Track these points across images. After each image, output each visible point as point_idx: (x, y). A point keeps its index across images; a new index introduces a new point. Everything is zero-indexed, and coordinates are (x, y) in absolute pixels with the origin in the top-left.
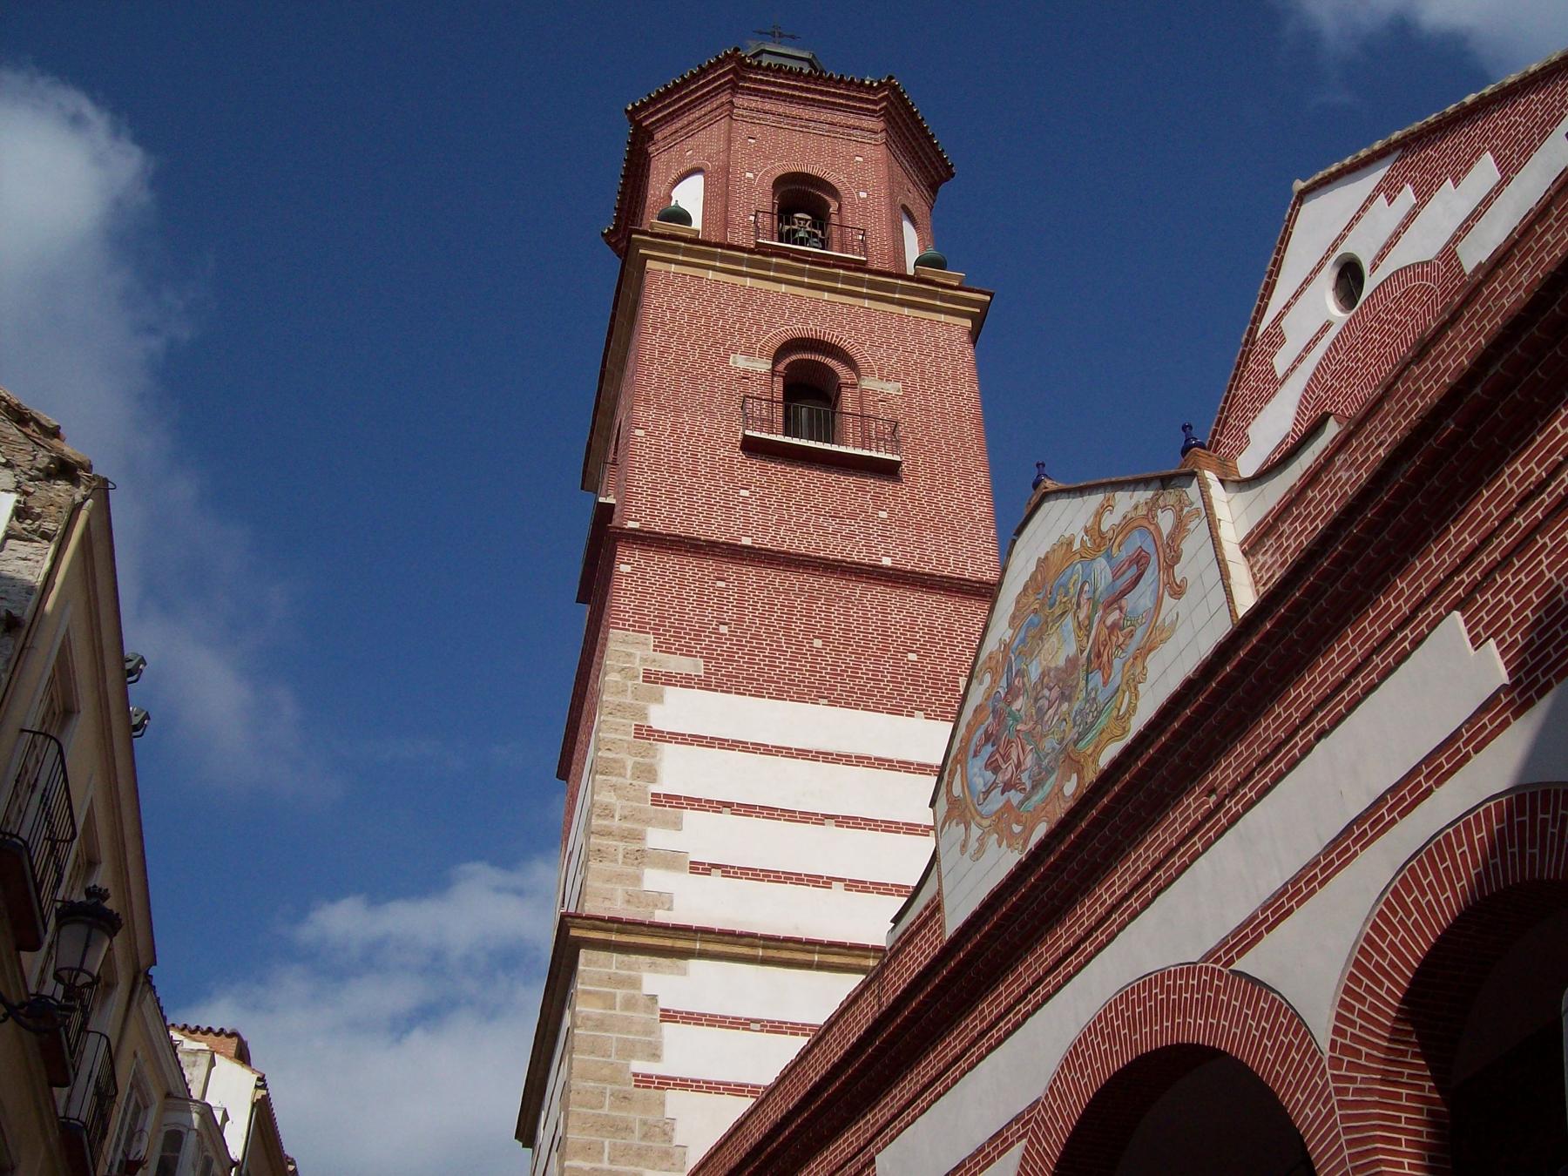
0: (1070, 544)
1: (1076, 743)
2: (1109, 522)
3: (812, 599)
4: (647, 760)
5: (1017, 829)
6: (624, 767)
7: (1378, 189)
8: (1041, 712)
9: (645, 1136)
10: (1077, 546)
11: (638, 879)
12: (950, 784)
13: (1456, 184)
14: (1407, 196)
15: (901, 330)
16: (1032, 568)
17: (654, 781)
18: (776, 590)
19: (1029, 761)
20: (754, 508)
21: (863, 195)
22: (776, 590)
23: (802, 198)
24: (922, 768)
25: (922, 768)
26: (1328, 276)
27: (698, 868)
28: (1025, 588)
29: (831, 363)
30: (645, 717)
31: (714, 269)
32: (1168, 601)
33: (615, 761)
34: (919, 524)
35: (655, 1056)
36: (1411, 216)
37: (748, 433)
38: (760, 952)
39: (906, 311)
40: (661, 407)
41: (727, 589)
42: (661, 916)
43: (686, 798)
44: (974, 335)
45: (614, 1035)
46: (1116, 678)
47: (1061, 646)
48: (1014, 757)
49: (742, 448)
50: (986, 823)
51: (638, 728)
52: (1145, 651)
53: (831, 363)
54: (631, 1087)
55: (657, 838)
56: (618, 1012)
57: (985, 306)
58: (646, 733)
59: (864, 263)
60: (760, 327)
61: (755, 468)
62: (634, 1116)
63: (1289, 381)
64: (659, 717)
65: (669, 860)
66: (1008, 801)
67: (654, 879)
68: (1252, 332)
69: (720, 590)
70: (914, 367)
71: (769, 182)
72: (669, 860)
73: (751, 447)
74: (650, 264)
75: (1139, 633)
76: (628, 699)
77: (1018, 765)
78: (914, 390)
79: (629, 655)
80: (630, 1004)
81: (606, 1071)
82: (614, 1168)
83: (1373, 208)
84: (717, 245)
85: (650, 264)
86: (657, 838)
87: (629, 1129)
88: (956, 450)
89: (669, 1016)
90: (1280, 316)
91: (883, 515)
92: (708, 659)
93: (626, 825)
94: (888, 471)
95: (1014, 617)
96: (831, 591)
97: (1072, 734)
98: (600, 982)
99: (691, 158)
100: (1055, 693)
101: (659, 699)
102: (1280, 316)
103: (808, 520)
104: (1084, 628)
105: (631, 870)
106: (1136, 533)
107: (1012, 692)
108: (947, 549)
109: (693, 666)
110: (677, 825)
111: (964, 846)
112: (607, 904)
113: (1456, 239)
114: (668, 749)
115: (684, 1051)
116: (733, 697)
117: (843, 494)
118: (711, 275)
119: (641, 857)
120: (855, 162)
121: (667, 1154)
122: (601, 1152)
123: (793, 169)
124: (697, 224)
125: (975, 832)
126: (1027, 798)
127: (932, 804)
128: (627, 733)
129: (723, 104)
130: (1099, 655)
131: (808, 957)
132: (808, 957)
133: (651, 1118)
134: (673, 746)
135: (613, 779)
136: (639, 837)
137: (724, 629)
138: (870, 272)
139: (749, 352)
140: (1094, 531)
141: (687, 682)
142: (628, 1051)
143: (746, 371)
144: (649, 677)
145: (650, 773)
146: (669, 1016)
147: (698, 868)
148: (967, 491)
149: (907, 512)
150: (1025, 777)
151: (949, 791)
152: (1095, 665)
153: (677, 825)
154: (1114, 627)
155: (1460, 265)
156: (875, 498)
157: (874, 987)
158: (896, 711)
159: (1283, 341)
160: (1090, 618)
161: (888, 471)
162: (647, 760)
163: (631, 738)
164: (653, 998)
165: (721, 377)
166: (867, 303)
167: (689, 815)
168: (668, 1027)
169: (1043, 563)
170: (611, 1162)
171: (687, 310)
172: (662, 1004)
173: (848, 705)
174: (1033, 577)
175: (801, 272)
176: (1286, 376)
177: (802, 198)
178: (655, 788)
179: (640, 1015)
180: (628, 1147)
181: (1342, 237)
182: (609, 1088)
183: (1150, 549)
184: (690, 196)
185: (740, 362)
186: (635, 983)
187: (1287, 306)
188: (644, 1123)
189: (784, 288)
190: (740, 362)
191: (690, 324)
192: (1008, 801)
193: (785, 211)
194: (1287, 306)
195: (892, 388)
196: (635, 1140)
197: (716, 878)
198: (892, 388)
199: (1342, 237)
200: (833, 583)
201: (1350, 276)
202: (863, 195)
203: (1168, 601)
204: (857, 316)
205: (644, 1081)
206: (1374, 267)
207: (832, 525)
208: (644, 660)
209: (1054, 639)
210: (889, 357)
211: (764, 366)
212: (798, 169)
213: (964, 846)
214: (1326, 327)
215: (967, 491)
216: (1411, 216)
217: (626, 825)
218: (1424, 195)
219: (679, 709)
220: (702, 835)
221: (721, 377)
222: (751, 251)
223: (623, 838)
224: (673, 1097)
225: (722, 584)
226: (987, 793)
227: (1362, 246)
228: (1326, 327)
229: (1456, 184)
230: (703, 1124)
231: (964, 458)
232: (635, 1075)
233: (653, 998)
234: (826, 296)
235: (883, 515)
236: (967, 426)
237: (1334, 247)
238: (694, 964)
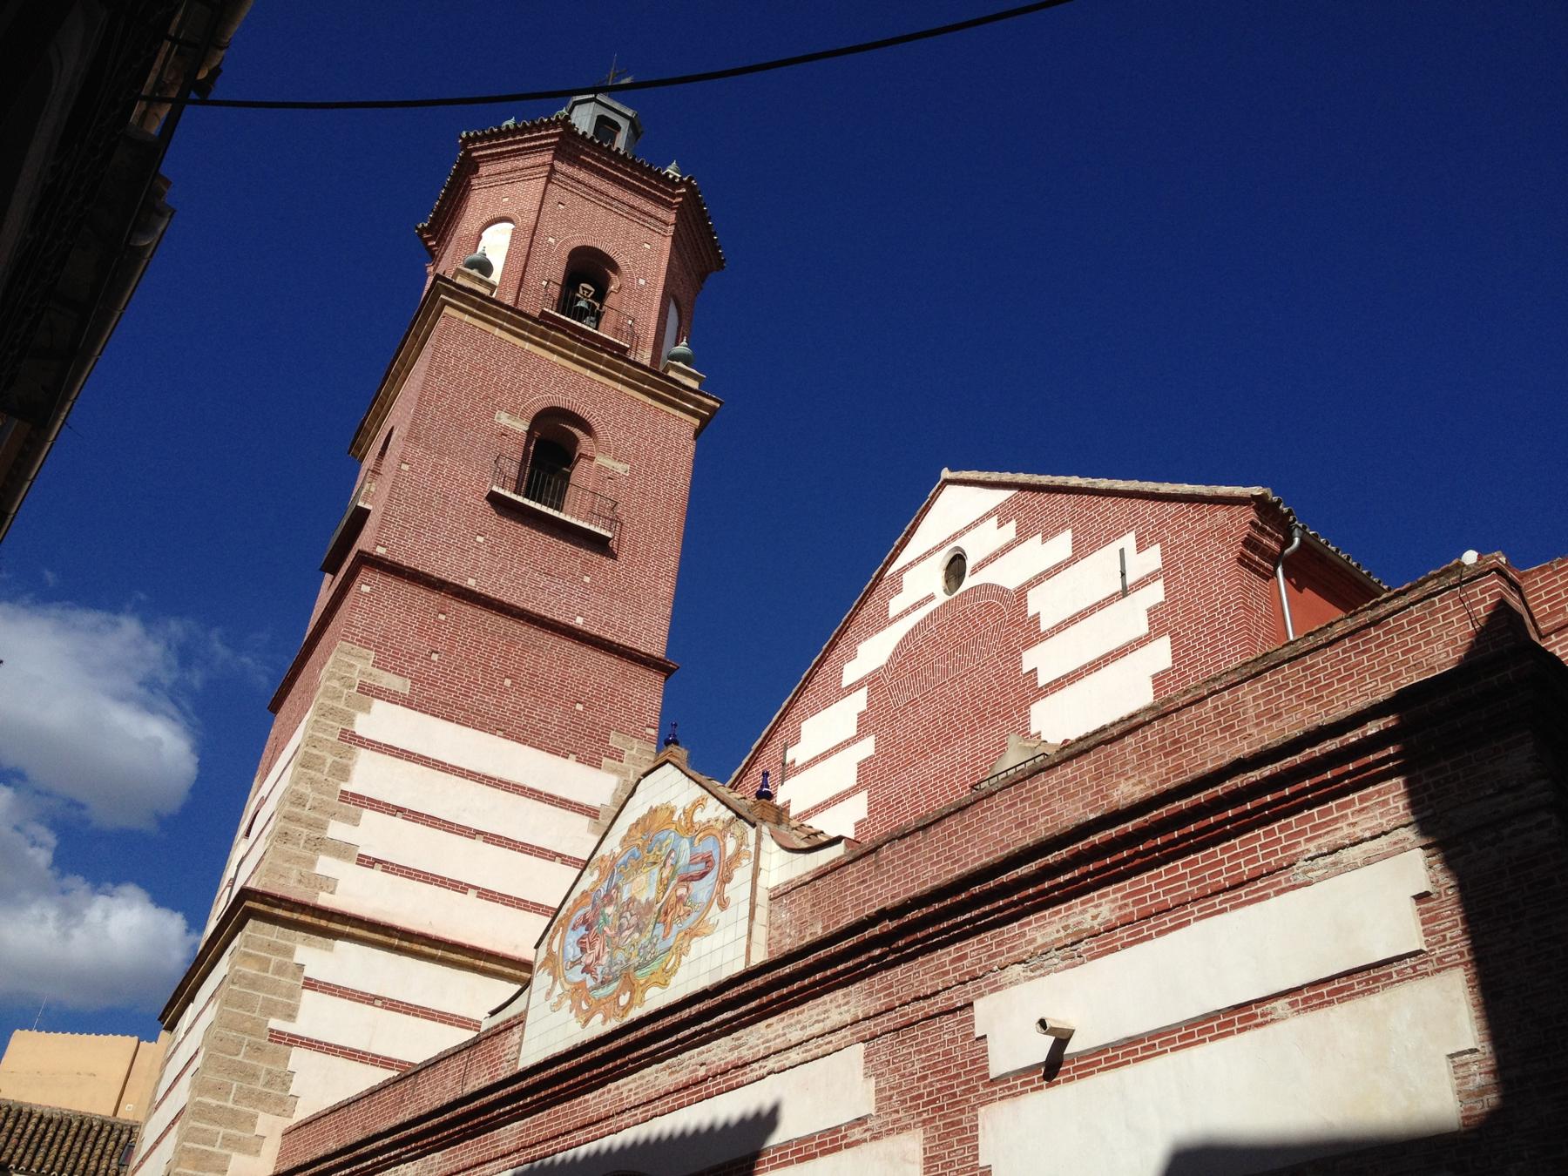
0: (672, 813)
1: (636, 969)
2: (700, 817)
3: (511, 643)
4: (344, 761)
5: (584, 1006)
6: (324, 764)
7: (995, 511)
8: (620, 929)
9: (269, 1084)
10: (675, 818)
11: (313, 863)
12: (552, 938)
13: (1044, 541)
14: (1010, 530)
15: (641, 418)
16: (645, 811)
17: (346, 780)
18: (485, 630)
19: (605, 959)
20: (484, 554)
21: (642, 282)
22: (485, 630)
23: (589, 270)
24: (536, 908)
25: (536, 908)
26: (941, 559)
27: (367, 862)
28: (637, 823)
29: (578, 432)
30: (351, 722)
31: (501, 327)
32: (715, 907)
33: (318, 757)
34: (613, 593)
35: (291, 1016)
36: (1008, 548)
37: (495, 489)
38: (396, 942)
39: (650, 401)
40: (428, 447)
41: (445, 622)
42: (324, 900)
43: (369, 799)
44: (698, 434)
45: (262, 995)
46: (671, 941)
47: (643, 888)
48: (597, 947)
49: (487, 498)
50: (567, 987)
51: (344, 731)
52: (691, 933)
53: (578, 432)
54: (264, 1041)
55: (337, 830)
56: (269, 975)
57: (713, 410)
58: (352, 739)
59: (625, 350)
60: (527, 391)
61: (492, 519)
62: (263, 1066)
63: (895, 625)
64: (364, 725)
65: (342, 851)
66: (584, 981)
67: (326, 865)
68: (884, 570)
69: (441, 622)
70: (642, 457)
71: (566, 251)
72: (342, 851)
73: (495, 500)
74: (447, 310)
75: (694, 915)
76: (341, 705)
77: (597, 958)
78: (639, 473)
79: (351, 666)
80: (281, 969)
81: (248, 1025)
82: (236, 1107)
83: (982, 526)
84: (508, 307)
85: (447, 310)
86: (337, 830)
87: (255, 1076)
88: (658, 533)
89: (311, 984)
90: (904, 569)
91: (587, 579)
92: (414, 681)
93: (313, 814)
94: (599, 544)
95: (624, 839)
96: (529, 638)
97: (635, 961)
98: (261, 948)
99: (505, 204)
100: (633, 920)
101: (367, 709)
102: (904, 569)
103: (526, 573)
104: (664, 885)
105: (308, 854)
106: (711, 839)
107: (609, 899)
108: (630, 619)
109: (399, 684)
110: (355, 821)
111: (549, 994)
112: (282, 881)
113: (1031, 584)
114: (363, 754)
115: (316, 1016)
116: (427, 717)
117: (560, 555)
118: (497, 331)
119: (320, 844)
120: (643, 250)
121: (281, 1102)
122: (228, 1093)
123: (589, 243)
124: (495, 277)
125: (558, 990)
126: (596, 988)
127: (537, 946)
128: (332, 734)
129: (544, 164)
130: (666, 914)
131: (434, 951)
132: (434, 951)
133: (274, 1068)
134: (368, 752)
135: (312, 773)
136: (322, 827)
137: (435, 657)
138: (629, 362)
139: (512, 413)
140: (689, 813)
141: (392, 698)
142: (270, 1009)
143: (506, 428)
144: (364, 689)
145: (343, 772)
146: (311, 984)
147: (367, 862)
148: (658, 571)
149: (607, 581)
150: (599, 970)
151: (550, 944)
152: (662, 918)
153: (355, 821)
154: (680, 899)
155: (1026, 606)
156: (584, 563)
157: (465, 1054)
158: (554, 751)
159: (900, 591)
160: (669, 879)
161: (599, 544)
162: (344, 761)
163: (334, 739)
164: (301, 967)
165: (484, 431)
166: (620, 387)
167: (367, 814)
168: (307, 993)
169: (653, 811)
170: (235, 1102)
171: (471, 359)
172: (307, 973)
173: (518, 740)
174: (644, 818)
175: (572, 348)
176: (895, 620)
177: (589, 270)
178: (345, 786)
179: (286, 980)
180: (251, 1092)
181: (960, 534)
182: (247, 1038)
183: (717, 859)
184: (496, 244)
185: (503, 419)
186: (289, 952)
187: (912, 564)
188: (269, 1072)
189: (555, 358)
190: (503, 419)
191: (469, 374)
192: (584, 981)
193: (572, 278)
194: (912, 564)
195: (621, 468)
196: (259, 1086)
197: (376, 874)
198: (621, 468)
199: (960, 534)
200: (532, 632)
201: (956, 568)
202: (642, 282)
203: (715, 907)
204: (609, 396)
205: (277, 1037)
206: (974, 571)
207: (544, 581)
208: (362, 673)
209: (643, 877)
210: (626, 439)
211: (522, 427)
212: (594, 244)
213: (549, 994)
214: (931, 598)
215: (658, 571)
216: (1008, 548)
217: (313, 814)
218: (1022, 536)
219: (383, 721)
220: (373, 833)
221: (484, 431)
222: (535, 320)
223: (309, 825)
224: (298, 1055)
225: (442, 617)
226: (574, 964)
227: (975, 548)
228: (931, 598)
229: (1044, 541)
230: (320, 1085)
231: (663, 541)
232: (272, 1030)
233: (301, 967)
234: (588, 373)
235: (587, 579)
236: (672, 514)
237: (954, 537)
238: (340, 945)
